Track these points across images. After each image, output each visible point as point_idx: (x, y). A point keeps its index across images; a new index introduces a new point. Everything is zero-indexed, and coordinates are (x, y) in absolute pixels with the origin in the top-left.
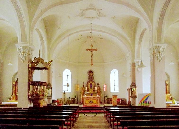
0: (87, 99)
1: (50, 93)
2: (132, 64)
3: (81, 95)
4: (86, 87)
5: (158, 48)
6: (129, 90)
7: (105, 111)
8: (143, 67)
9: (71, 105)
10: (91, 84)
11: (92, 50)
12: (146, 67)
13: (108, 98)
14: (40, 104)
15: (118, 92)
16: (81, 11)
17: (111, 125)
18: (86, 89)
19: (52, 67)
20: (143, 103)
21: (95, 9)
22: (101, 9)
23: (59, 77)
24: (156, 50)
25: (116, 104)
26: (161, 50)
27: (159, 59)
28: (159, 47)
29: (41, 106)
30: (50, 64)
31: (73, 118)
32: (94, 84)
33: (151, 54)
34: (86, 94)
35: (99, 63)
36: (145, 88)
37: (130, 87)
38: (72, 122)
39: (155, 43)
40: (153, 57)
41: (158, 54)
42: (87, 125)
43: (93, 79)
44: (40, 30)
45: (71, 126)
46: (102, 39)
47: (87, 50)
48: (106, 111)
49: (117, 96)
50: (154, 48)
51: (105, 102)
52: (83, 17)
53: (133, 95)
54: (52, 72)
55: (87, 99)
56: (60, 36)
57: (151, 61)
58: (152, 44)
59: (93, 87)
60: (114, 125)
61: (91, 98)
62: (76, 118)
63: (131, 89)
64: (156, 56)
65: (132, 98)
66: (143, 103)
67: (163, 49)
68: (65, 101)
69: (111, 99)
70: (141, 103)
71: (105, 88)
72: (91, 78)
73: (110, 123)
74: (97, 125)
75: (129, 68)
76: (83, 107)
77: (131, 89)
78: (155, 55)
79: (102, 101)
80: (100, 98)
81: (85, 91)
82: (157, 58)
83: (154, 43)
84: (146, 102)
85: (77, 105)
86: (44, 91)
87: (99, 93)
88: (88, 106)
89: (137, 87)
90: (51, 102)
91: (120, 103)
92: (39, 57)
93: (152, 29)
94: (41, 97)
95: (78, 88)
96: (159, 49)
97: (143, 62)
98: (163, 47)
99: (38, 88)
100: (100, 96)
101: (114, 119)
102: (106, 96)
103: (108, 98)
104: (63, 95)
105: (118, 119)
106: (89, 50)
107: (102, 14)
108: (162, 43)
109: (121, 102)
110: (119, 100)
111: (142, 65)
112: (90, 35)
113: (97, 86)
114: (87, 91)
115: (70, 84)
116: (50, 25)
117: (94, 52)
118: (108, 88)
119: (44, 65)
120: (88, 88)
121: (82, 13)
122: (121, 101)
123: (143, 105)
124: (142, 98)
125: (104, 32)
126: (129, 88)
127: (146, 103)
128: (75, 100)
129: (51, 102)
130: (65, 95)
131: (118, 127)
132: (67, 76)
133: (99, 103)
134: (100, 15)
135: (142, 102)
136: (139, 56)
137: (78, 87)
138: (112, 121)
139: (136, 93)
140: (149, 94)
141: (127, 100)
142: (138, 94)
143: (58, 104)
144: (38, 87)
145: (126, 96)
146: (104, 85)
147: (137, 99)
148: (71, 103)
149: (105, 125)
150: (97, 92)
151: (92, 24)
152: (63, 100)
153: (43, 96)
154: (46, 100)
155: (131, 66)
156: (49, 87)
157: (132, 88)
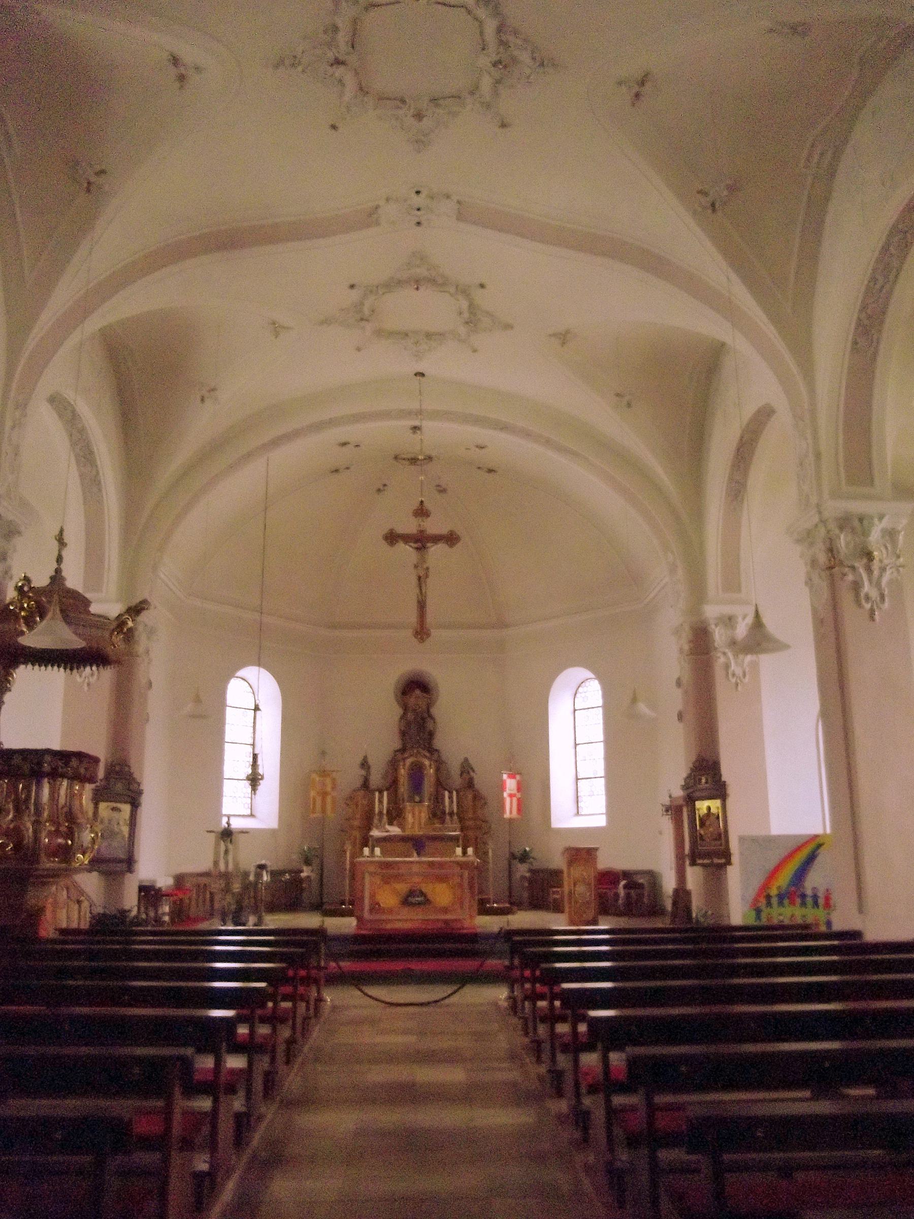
0: (386, 880)
1: (125, 830)
2: (686, 634)
3: (348, 847)
4: (381, 792)
5: (853, 530)
6: (674, 811)
7: (511, 968)
8: (765, 651)
9: (274, 921)
10: (418, 771)
11: (421, 541)
12: (787, 647)
13: (536, 865)
14: (36, 915)
15: (601, 821)
16: (355, 295)
17: (557, 1075)
18: (381, 802)
19: (147, 652)
20: (775, 901)
21: (444, 284)
22: (482, 286)
23: (193, 716)
24: (843, 542)
25: (590, 915)
26: (875, 536)
27: (867, 598)
28: (861, 520)
29: (47, 931)
30: (130, 624)
31: (274, 1030)
32: (438, 770)
33: (814, 563)
34: (380, 841)
35: (470, 627)
36: (785, 793)
37: (685, 787)
38: (263, 1063)
39: (836, 495)
40: (824, 585)
41: (856, 565)
42: (379, 1075)
43: (431, 734)
44: (84, 409)
45: (273, 1059)
46: (490, 471)
47: (392, 538)
48: (524, 966)
49: (599, 854)
50: (832, 526)
51: (510, 896)
52: (363, 328)
53: (707, 848)
54: (144, 681)
55: (388, 873)
56: (215, 447)
57: (815, 612)
58: (814, 499)
59: (428, 786)
60: (577, 1085)
61: (415, 869)
62: (312, 1003)
63: (690, 800)
64: (850, 577)
65: (695, 868)
66: (781, 903)
67: (891, 534)
68: (227, 890)
69: (557, 873)
70: (763, 902)
71: (511, 796)
73: (545, 1056)
74: (454, 1075)
75: (671, 660)
76: (357, 939)
77: (690, 800)
78: (844, 575)
79: (495, 886)
80: (479, 871)
81: (376, 821)
82: (857, 595)
83: (826, 496)
84: (795, 893)
85: (309, 920)
86: (71, 817)
87: (471, 834)
88: (389, 926)
89: (731, 790)
90: (130, 900)
91: (620, 902)
92: (57, 578)
93: (813, 412)
94: (48, 864)
95: (324, 794)
96: (866, 533)
97: (766, 620)
98: (885, 523)
99: (28, 797)
100: (476, 852)
101: (533, 986)
102: (517, 850)
103: (530, 871)
104: (217, 845)
105: (606, 1036)
106: (406, 538)
107: (489, 314)
108: (880, 499)
109: (628, 896)
110: (609, 878)
111: (759, 639)
112: (412, 444)
113: (457, 780)
114: (385, 818)
115: (270, 767)
116: (146, 380)
117: (436, 551)
118: (536, 789)
119: (79, 635)
120: (395, 801)
121: (362, 304)
122: (622, 892)
123: (775, 921)
124: (771, 865)
125: (504, 427)
126: (679, 793)
127: (798, 901)
128: (301, 881)
129: (130, 900)
130: (230, 847)
131: (608, 1101)
132: (253, 713)
133: (471, 907)
134: (473, 318)
135: (774, 892)
136: (732, 581)
137: (329, 789)
138: (563, 1051)
139: (726, 831)
140: (816, 836)
141: (669, 884)
142: (742, 839)
143: (179, 913)
144: (27, 788)
145: (656, 854)
146: (505, 776)
147: (734, 875)
148: (273, 908)
149: (509, 1074)
150: (457, 825)
151: (423, 375)
152: (220, 884)
153: (65, 853)
154: (90, 883)
155: (686, 647)
156: (119, 787)
157: (698, 794)
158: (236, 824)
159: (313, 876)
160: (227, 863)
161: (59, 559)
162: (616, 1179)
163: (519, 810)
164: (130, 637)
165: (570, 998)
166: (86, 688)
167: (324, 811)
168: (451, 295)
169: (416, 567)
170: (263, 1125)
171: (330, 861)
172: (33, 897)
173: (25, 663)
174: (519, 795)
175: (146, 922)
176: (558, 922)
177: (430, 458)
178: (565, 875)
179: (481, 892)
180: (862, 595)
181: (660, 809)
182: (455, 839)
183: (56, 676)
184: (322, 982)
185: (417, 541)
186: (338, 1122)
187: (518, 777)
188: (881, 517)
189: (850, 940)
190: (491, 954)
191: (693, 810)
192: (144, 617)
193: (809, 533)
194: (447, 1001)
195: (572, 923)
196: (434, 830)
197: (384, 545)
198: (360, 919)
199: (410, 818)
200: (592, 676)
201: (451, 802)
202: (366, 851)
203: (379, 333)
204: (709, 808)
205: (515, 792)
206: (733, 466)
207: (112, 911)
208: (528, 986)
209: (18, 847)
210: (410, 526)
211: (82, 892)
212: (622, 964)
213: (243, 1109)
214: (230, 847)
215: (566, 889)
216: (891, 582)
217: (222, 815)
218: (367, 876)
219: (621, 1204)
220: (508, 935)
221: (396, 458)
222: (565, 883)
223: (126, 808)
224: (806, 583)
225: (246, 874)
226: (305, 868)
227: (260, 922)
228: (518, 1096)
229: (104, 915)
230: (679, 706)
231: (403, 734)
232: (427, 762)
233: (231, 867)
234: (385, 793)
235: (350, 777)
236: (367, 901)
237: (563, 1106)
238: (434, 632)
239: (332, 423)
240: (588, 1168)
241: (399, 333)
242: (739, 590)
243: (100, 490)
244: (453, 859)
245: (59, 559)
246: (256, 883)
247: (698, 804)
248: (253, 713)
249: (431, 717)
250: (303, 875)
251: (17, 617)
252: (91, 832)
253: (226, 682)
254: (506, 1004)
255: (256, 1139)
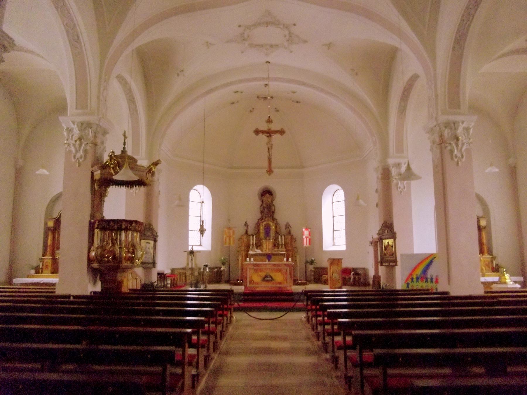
0: (256, 271)
1: (152, 251)
3: (240, 258)
4: (253, 236)
5: (451, 129)
6: (374, 243)
7: (307, 305)
8: (413, 179)
9: (211, 287)
11: (269, 133)
13: (317, 266)
14: (120, 283)
15: (344, 248)
17: (325, 345)
18: (253, 240)
19: (158, 180)
20: (415, 280)
21: (279, 24)
22: (294, 25)
24: (446, 133)
26: (460, 131)
27: (456, 156)
28: (454, 124)
29: (125, 289)
30: (154, 169)
31: (216, 326)
32: (276, 227)
33: (434, 142)
34: (252, 255)
37: (379, 234)
40: (438, 151)
41: (452, 142)
43: (273, 212)
44: (128, 78)
46: (298, 102)
49: (343, 261)
50: (441, 126)
53: (387, 259)
55: (257, 268)
59: (272, 234)
61: (268, 266)
64: (449, 148)
66: (417, 281)
67: (467, 129)
68: (192, 274)
70: (410, 281)
71: (306, 237)
72: (268, 210)
73: (321, 338)
74: (285, 345)
75: (373, 180)
76: (244, 294)
77: (381, 240)
79: (299, 275)
81: (251, 247)
84: (423, 277)
86: (133, 246)
87: (290, 253)
88: (258, 289)
89: (398, 235)
90: (154, 278)
91: (351, 280)
92: (124, 151)
94: (126, 264)
95: (230, 237)
96: (456, 129)
97: (412, 166)
98: (465, 125)
99: (117, 239)
100: (292, 260)
102: (309, 259)
103: (315, 268)
105: (345, 328)
106: (263, 132)
108: (463, 115)
109: (354, 278)
110: (346, 271)
111: (409, 175)
113: (284, 231)
114: (255, 246)
115: (208, 226)
119: (136, 174)
122: (352, 277)
123: (415, 288)
125: (303, 84)
126: (376, 236)
127: (425, 280)
128: (221, 271)
129: (154, 278)
130: (193, 258)
132: (200, 204)
135: (415, 277)
140: (432, 255)
141: (372, 273)
142: (402, 255)
143: (173, 284)
145: (366, 261)
146: (304, 230)
147: (398, 269)
148: (210, 282)
149: (307, 344)
151: (269, 62)
153: (132, 260)
154: (139, 271)
155: (380, 176)
156: (149, 234)
158: (195, 249)
159: (226, 269)
160: (192, 264)
161: (124, 144)
162: (348, 380)
163: (310, 244)
164: (153, 174)
165: (330, 315)
166: (134, 195)
167: (230, 243)
168: (281, 29)
169: (267, 144)
170: (214, 361)
171: (232, 263)
172: (120, 276)
173: (113, 185)
174: (310, 237)
175: (161, 287)
176: (325, 288)
177: (272, 97)
178: (329, 269)
179: (294, 276)
180: (454, 155)
181: (368, 243)
182: (283, 255)
183: (123, 190)
184: (232, 311)
185: (268, 133)
186: (241, 361)
187: (309, 230)
188: (463, 123)
189: (445, 297)
190: (297, 301)
191: (382, 243)
192: (159, 166)
193: (432, 129)
194: (281, 318)
195: (331, 288)
196: (275, 251)
197: (254, 135)
198: (246, 287)
199: (265, 246)
200: (340, 188)
201: (282, 240)
202: (248, 259)
203: (251, 45)
204: (388, 243)
205: (308, 236)
206: (401, 100)
207: (148, 282)
208: (314, 312)
209: (114, 257)
210: (264, 127)
211: (137, 275)
212: (352, 320)
213: (207, 354)
214: (193, 258)
215: (329, 275)
216: (466, 149)
217: (188, 245)
218: (248, 270)
219: (350, 389)
220: (306, 293)
221: (258, 97)
222: (329, 273)
223: (152, 242)
224: (431, 150)
225: (200, 269)
226: (222, 266)
227: (206, 287)
228: (309, 352)
229: (145, 284)
230: (376, 201)
231: (262, 212)
232: (271, 224)
233: (194, 266)
234: (255, 236)
235: (241, 230)
236: (248, 280)
237: (328, 356)
238: (275, 171)
239: (231, 84)
240: (337, 377)
241: (259, 45)
242: (402, 152)
243: (137, 114)
244: (283, 263)
245: (124, 144)
246: (203, 272)
247: (384, 241)
248: (200, 204)
249: (273, 205)
250: (222, 269)
251: (110, 167)
252: (141, 251)
253: (189, 191)
254: (305, 319)
255: (212, 365)
